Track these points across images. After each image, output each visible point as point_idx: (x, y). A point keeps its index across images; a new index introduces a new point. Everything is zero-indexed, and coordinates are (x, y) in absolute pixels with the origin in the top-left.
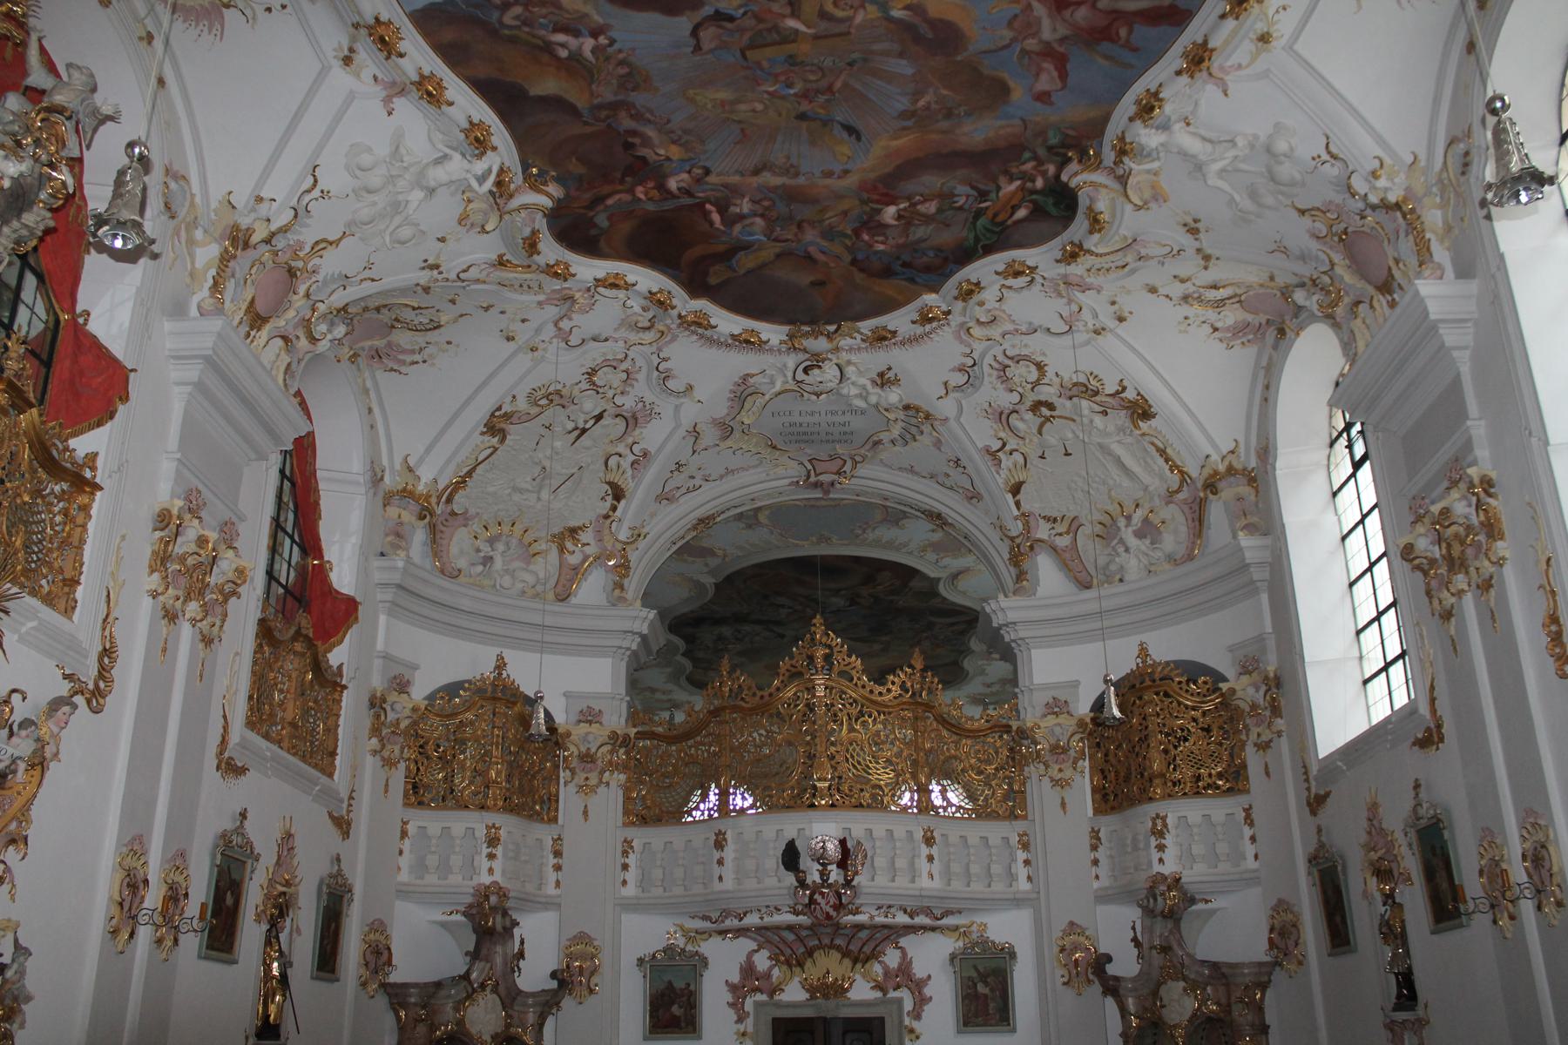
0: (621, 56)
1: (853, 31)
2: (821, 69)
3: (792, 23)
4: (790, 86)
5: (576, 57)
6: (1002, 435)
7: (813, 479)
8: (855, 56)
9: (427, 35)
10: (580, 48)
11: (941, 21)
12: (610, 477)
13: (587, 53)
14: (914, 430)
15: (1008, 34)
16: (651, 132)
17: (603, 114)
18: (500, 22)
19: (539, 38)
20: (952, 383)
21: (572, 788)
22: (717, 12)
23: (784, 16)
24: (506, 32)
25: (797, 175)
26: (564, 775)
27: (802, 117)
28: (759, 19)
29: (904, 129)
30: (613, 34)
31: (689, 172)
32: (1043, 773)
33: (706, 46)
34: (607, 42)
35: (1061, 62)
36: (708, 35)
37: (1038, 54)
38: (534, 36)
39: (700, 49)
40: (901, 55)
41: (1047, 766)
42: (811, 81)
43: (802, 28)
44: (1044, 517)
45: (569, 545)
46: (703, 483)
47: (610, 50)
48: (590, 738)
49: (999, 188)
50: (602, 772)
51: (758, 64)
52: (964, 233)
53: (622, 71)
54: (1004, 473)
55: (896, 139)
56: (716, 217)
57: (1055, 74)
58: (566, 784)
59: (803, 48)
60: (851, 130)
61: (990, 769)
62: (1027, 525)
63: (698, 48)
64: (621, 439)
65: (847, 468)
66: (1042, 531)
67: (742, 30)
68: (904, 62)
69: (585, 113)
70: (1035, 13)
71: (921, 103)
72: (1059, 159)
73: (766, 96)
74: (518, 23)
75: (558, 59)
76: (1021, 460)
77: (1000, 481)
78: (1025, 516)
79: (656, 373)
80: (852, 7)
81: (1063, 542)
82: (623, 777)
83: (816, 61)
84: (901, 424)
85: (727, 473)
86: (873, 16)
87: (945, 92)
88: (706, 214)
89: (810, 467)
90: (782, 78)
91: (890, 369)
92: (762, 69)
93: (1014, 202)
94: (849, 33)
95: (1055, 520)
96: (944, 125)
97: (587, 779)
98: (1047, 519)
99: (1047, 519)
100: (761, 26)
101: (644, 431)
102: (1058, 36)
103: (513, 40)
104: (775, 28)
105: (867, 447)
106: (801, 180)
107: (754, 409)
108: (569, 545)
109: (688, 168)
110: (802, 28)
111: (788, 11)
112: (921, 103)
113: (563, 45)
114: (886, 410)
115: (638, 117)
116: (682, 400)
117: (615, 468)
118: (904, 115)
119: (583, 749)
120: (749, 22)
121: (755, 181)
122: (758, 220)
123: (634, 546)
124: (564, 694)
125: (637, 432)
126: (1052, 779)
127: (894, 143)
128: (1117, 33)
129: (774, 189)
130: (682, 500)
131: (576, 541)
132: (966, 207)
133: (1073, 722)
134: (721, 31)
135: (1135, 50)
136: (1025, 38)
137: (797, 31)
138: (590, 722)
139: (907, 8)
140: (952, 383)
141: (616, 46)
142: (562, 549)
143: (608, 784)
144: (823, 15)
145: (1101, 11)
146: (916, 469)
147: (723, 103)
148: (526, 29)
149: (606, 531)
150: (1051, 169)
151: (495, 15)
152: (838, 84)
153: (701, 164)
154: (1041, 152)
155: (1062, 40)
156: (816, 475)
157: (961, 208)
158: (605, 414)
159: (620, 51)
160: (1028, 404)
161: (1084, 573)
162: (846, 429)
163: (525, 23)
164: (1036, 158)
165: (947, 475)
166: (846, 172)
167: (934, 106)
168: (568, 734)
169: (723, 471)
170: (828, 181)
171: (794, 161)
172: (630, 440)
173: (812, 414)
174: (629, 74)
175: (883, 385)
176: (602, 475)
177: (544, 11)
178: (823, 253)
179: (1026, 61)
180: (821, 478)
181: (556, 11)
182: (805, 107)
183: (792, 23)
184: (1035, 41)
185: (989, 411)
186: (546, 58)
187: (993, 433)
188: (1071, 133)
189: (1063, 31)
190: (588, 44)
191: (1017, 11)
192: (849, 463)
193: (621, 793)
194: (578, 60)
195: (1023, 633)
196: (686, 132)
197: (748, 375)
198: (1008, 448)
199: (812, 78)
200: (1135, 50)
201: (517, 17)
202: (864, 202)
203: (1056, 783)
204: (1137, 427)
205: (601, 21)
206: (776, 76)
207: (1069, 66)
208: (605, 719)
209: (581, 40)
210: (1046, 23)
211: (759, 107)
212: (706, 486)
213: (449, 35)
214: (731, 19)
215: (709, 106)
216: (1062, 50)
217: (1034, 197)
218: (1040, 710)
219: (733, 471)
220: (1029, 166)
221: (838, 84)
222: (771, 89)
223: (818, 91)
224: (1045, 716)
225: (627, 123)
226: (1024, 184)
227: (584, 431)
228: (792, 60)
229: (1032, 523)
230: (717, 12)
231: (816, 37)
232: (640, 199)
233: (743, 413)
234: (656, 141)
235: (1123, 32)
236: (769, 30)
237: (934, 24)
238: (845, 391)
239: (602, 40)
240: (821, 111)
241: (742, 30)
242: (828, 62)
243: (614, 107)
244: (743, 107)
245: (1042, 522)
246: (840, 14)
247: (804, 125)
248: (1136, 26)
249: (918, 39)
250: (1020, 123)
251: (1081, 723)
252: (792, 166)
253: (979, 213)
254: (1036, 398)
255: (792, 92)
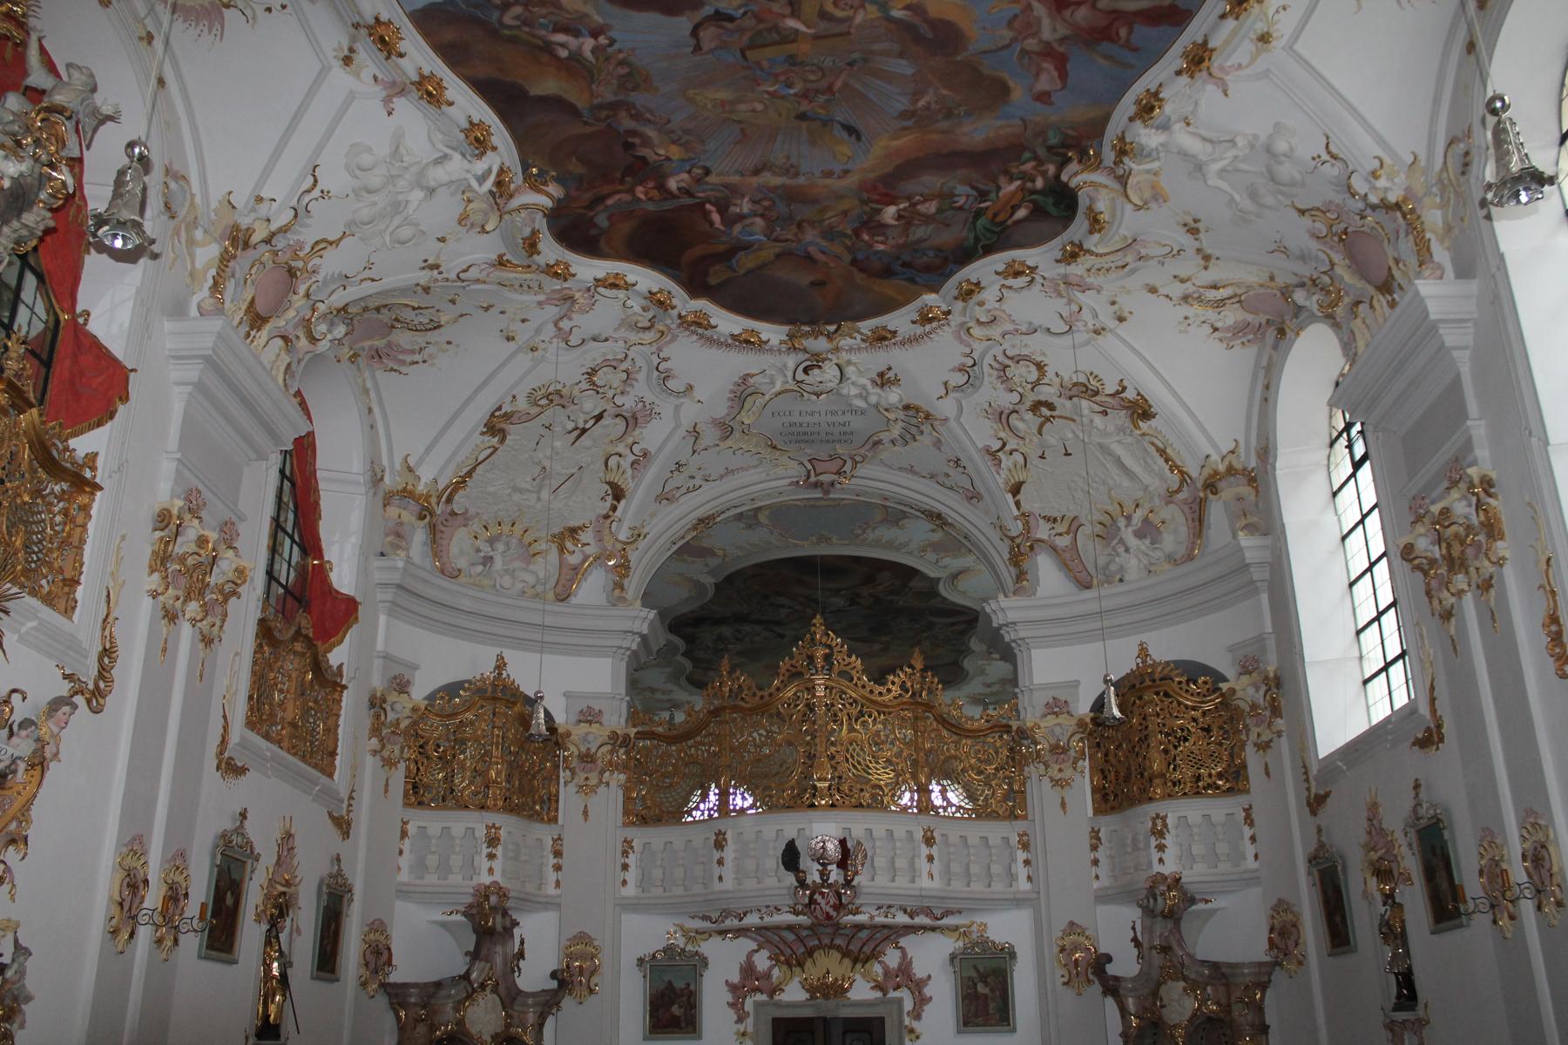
0: (621, 56)
1: (853, 31)
2: (821, 69)
3: (792, 23)
4: (790, 86)
5: (576, 57)
6: (1002, 435)
7: (813, 479)
8: (855, 56)
9: (427, 35)
10: (580, 48)
11: (941, 21)
12: (611, 477)
13: (587, 53)
14: (914, 430)
15: (1008, 34)
16: (651, 132)
17: (603, 114)
18: (500, 22)
19: (539, 38)
20: (952, 383)
21: (572, 788)
22: (717, 12)
23: (784, 16)
24: (506, 32)
25: (797, 175)
26: (564, 775)
27: (802, 117)
28: (760, 20)
29: (904, 129)
30: (614, 34)
31: (689, 172)
32: (1043, 773)
33: (706, 46)
34: (606, 42)
35: (1061, 62)
36: (708, 35)
37: (1039, 54)
38: (534, 36)
39: (700, 49)
40: (901, 55)
41: (1047, 766)
42: (811, 81)
43: (802, 28)
44: (1044, 517)
45: (569, 545)
46: (703, 483)
47: (610, 50)
48: (590, 738)
49: (999, 188)
50: (602, 773)
51: (759, 64)
52: (964, 233)
53: (622, 71)
54: (1004, 473)
55: (896, 139)
56: (716, 217)
57: (1055, 74)
58: (566, 783)
59: (803, 48)
60: (851, 130)
61: (990, 769)
62: (1027, 525)
63: (698, 48)
64: (621, 439)
65: (847, 468)
66: (1042, 531)
67: (742, 30)
68: (904, 62)
69: (585, 113)
70: (1035, 13)
71: (921, 103)
72: (1059, 159)
73: (766, 96)
74: (518, 23)
75: (558, 59)
76: (1021, 460)
77: (1000, 481)
78: (1025, 516)
79: (656, 373)
80: (852, 7)
81: (1063, 542)
82: (622, 777)
83: (816, 61)
84: (901, 424)
85: (727, 474)
86: (872, 16)
87: (945, 92)
88: (706, 214)
89: (810, 467)
90: (782, 78)
91: (890, 369)
92: (762, 70)
93: (1014, 202)
94: (848, 33)
95: (1055, 520)
96: (944, 125)
97: (587, 779)
98: (1047, 519)
99: (1047, 519)
100: (761, 26)
101: (644, 431)
102: (1058, 36)
103: (512, 40)
104: (775, 28)
105: (867, 447)
106: (801, 180)
107: (754, 409)
108: (569, 545)
109: (688, 168)
110: (802, 28)
111: (788, 11)
112: (921, 103)
113: (563, 45)
114: (886, 410)
115: (638, 117)
116: (682, 400)
117: (615, 467)
118: (904, 115)
119: (583, 749)
120: (749, 22)
121: (755, 181)
122: (758, 220)
123: (634, 546)
124: (564, 695)
125: (637, 432)
126: (1052, 779)
127: (895, 143)
128: (1117, 33)
129: (774, 189)
130: (682, 500)
131: (576, 541)
132: (966, 207)
133: (1073, 722)
134: (721, 31)
135: (1135, 50)
136: (1025, 38)
137: (797, 31)
138: (590, 722)
139: (907, 8)
140: (952, 383)
141: (616, 46)
142: (562, 549)
143: (608, 784)
144: (823, 15)
145: (1101, 11)
146: (916, 469)
147: (723, 103)
148: (526, 29)
149: (606, 532)
150: (1051, 169)
151: (496, 15)
152: (838, 84)
153: (701, 164)
154: (1041, 152)
155: (1062, 40)
156: (816, 475)
157: (961, 208)
158: (605, 414)
159: (620, 51)
160: (1028, 404)
161: (1084, 573)
162: (846, 429)
163: (525, 23)
164: (1035, 158)
165: (947, 475)
166: (846, 172)
167: (934, 106)
168: (568, 734)
169: (723, 471)
170: (828, 181)
171: (794, 161)
172: (630, 440)
173: (812, 414)
174: (629, 74)
175: (883, 385)
176: (602, 475)
177: (544, 11)
178: (823, 253)
179: (1026, 61)
180: (821, 478)
181: (556, 11)
182: (805, 107)
183: (792, 23)
184: (1034, 41)
185: (990, 411)
186: (545, 58)
187: (993, 433)
188: (1071, 133)
189: (1063, 31)
190: (588, 44)
191: (1018, 11)
192: (849, 463)
193: (620, 793)
194: (578, 60)
195: (1023, 633)
196: (686, 132)
197: (748, 375)
198: (1008, 448)
199: (812, 78)
200: (1135, 50)
201: (517, 17)
202: (864, 202)
203: (1056, 783)
204: (1137, 427)
205: (601, 20)
206: (776, 76)
207: (1068, 66)
208: (605, 719)
209: (581, 40)
210: (1046, 23)
211: (759, 107)
212: (706, 486)
213: (449, 35)
214: (731, 19)
215: (709, 106)
216: (1062, 49)
217: (1034, 197)
218: (1040, 710)
219: (733, 471)
220: (1029, 166)
221: (838, 84)
222: (771, 89)
223: (817, 91)
224: (1045, 716)
225: (627, 123)
226: (1024, 184)
227: (584, 431)
228: (792, 60)
229: (1032, 523)
230: (717, 12)
231: (816, 37)
232: (640, 199)
233: (743, 413)
234: (656, 141)
235: (1123, 32)
236: (769, 30)
237: (934, 24)
238: (845, 391)
239: (602, 40)
240: (821, 111)
241: (742, 30)
242: (828, 63)
243: (614, 107)
244: (743, 107)
245: (1042, 522)
246: (840, 14)
247: (804, 125)
248: (1136, 26)
249: (918, 39)
250: (1020, 123)
251: (1081, 724)
252: (792, 166)
253: (979, 213)
254: (1036, 398)
255: (792, 92)
